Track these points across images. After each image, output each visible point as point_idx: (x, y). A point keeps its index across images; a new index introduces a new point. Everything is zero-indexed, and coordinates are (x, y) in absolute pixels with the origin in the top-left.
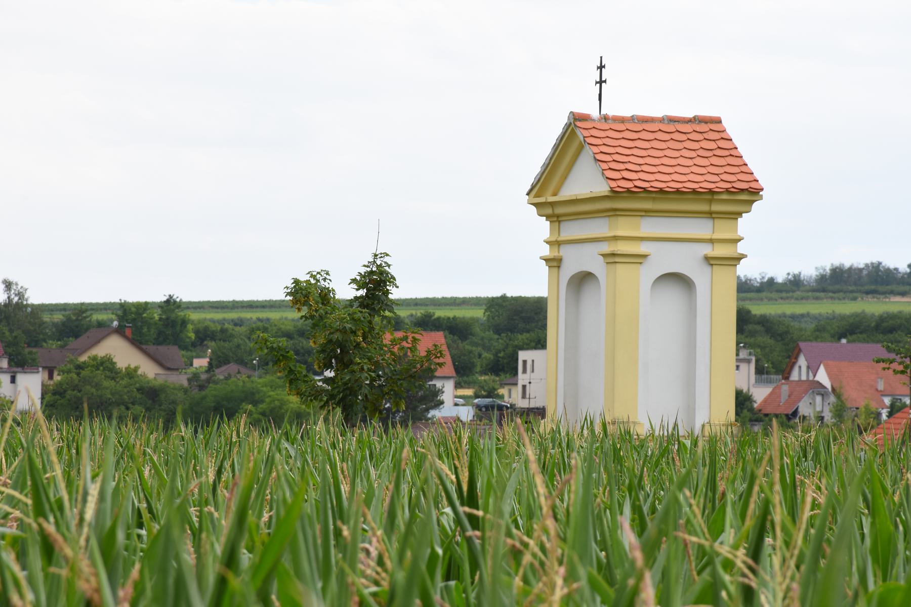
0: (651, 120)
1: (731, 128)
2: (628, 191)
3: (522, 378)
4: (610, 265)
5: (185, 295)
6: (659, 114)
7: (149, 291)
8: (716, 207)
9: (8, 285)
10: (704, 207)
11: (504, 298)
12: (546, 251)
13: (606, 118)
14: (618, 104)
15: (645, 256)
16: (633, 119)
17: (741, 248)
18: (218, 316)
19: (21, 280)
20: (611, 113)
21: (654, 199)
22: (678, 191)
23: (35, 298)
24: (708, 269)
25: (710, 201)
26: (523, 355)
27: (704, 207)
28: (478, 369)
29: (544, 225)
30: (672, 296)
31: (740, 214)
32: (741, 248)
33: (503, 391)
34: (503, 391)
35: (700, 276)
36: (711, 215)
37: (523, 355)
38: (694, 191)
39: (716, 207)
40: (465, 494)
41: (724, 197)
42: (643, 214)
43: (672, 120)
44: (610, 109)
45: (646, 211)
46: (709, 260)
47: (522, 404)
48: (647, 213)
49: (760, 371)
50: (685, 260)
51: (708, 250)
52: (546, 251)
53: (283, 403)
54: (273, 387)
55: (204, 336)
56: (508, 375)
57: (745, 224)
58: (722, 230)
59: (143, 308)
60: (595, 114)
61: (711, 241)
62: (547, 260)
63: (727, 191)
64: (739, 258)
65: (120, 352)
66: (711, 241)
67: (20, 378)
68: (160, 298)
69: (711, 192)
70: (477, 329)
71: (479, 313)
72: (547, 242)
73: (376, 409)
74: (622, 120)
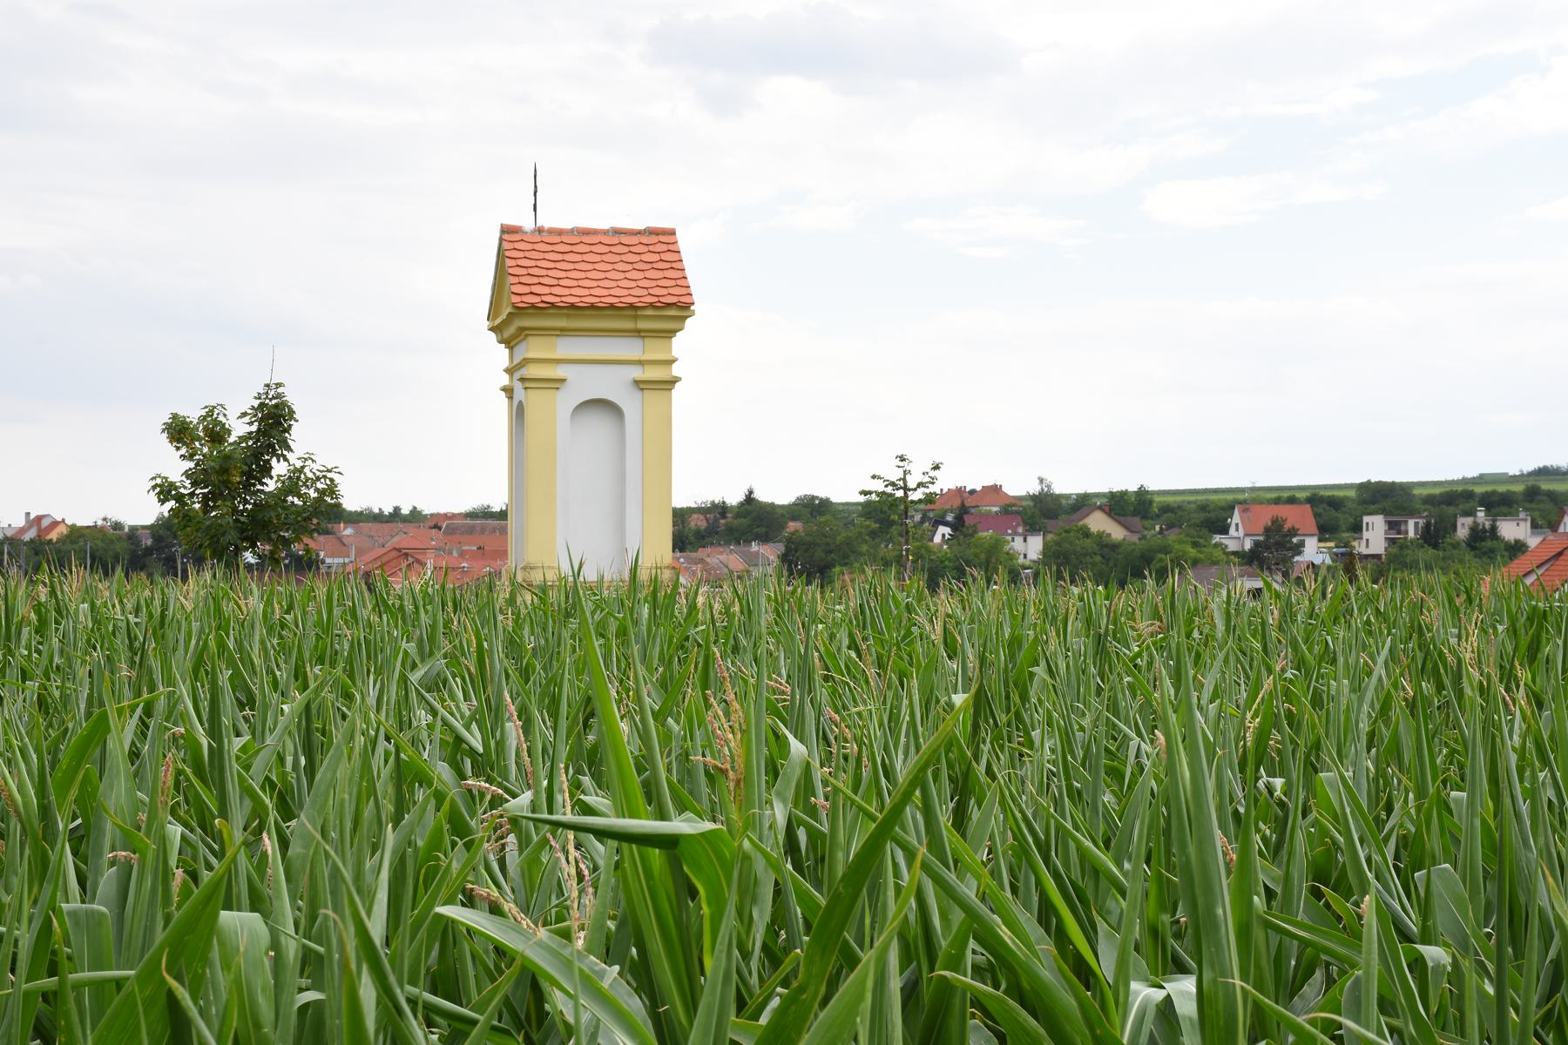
1: (684, 242)
2: (533, 306)
3: (1366, 535)
5: (1152, 486)
6: (605, 226)
7: (1127, 482)
8: (642, 325)
9: (1041, 481)
10: (629, 325)
11: (1369, 482)
12: (505, 380)
13: (540, 230)
15: (563, 381)
16: (571, 231)
17: (676, 370)
18: (1179, 498)
19: (1049, 478)
20: (547, 225)
21: (568, 316)
22: (593, 307)
23: (1058, 489)
24: (639, 394)
25: (636, 318)
26: (1366, 519)
27: (629, 325)
28: (1344, 527)
29: (502, 352)
30: (597, 427)
31: (674, 332)
32: (676, 370)
33: (1355, 544)
34: (1355, 544)
36: (638, 333)
37: (1366, 519)
38: (612, 306)
39: (642, 325)
41: (650, 312)
43: (617, 232)
44: (546, 221)
45: (562, 330)
46: (639, 384)
47: (1365, 551)
48: (563, 332)
49: (1534, 526)
50: (610, 384)
53: (1185, 553)
54: (1181, 542)
55: (1166, 509)
56: (166, 514)
57: (679, 343)
58: (653, 350)
59: (1124, 494)
60: (528, 225)
61: (641, 363)
62: (504, 389)
63: (651, 305)
64: (673, 382)
65: (1098, 523)
66: (641, 363)
67: (1029, 539)
68: (1133, 488)
69: (632, 306)
70: (1349, 504)
71: (1352, 494)
74: (560, 232)
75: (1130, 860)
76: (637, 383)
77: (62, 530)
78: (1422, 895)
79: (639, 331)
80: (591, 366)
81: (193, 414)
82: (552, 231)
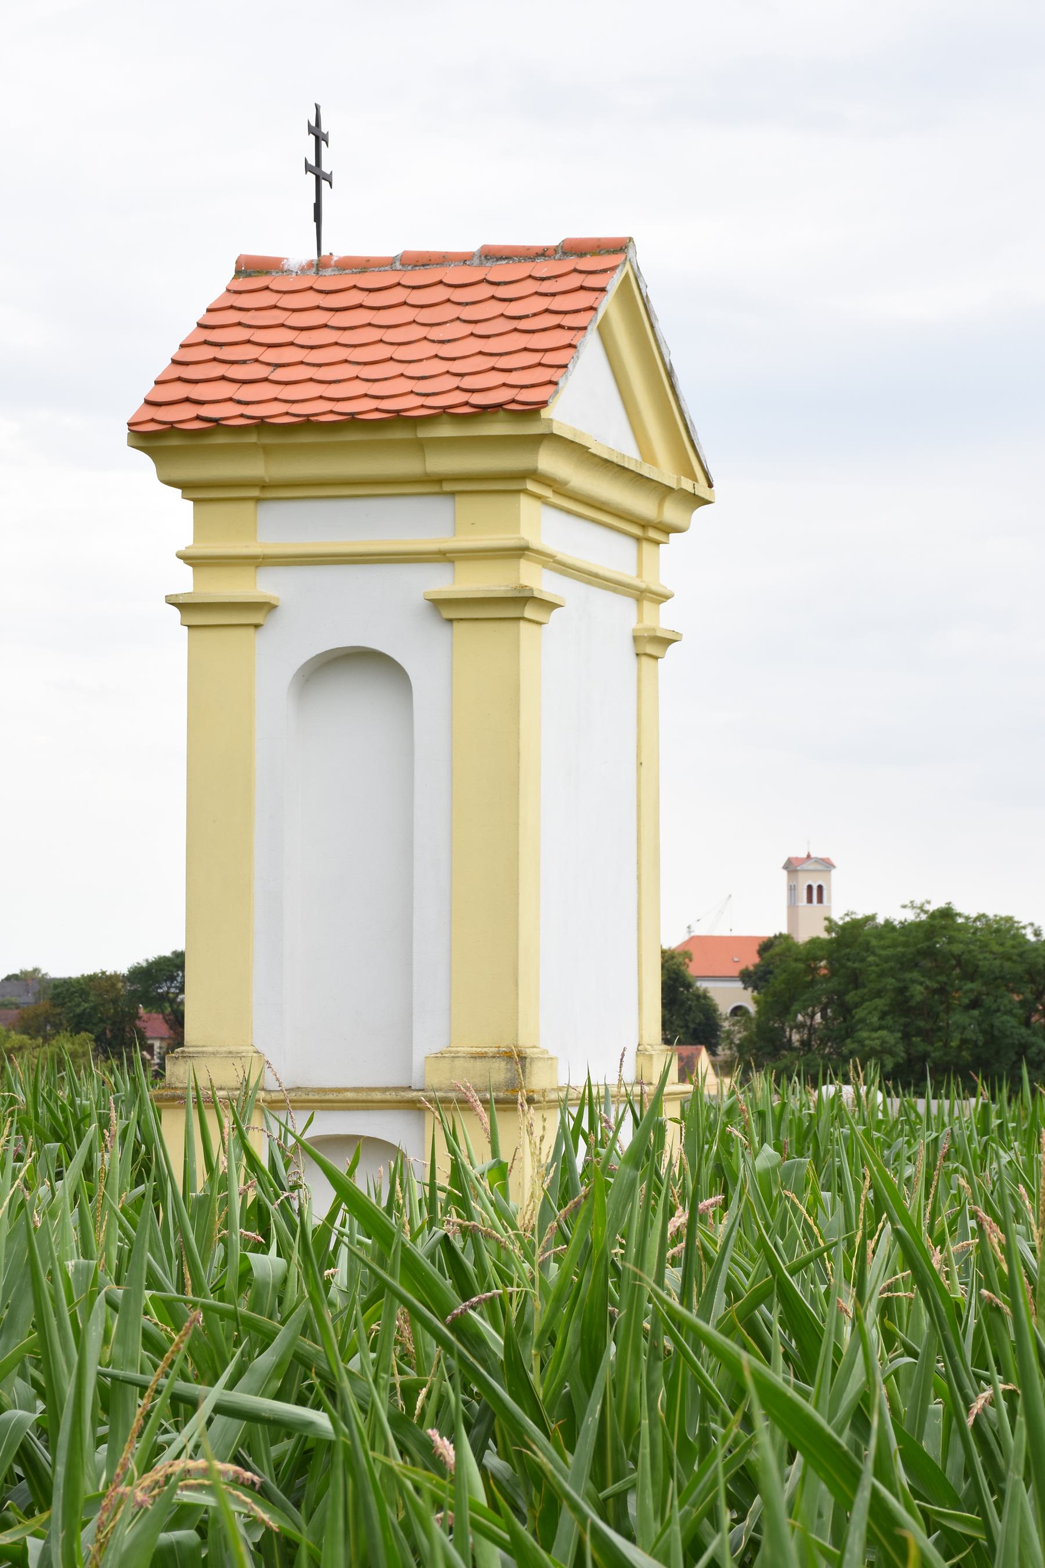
0: (442, 260)
4: (199, 634)
8: (440, 463)
14: (364, 229)
15: (267, 607)
24: (440, 635)
25: (421, 446)
29: (175, 516)
30: (355, 708)
35: (423, 652)
36: (437, 485)
40: (861, 1347)
41: (446, 431)
42: (255, 493)
43: (491, 255)
44: (337, 247)
46: (447, 610)
48: (266, 491)
50: (378, 610)
51: (444, 582)
52: (184, 581)
60: (297, 250)
61: (445, 557)
62: (184, 606)
63: (445, 413)
66: (445, 557)
72: (186, 558)
73: (97, 1046)
74: (364, 266)
75: (645, 1330)
76: (438, 604)
77: (684, 1156)
78: (309, 1267)
79: (439, 480)
80: (356, 567)
81: (907, 903)
82: (347, 265)
